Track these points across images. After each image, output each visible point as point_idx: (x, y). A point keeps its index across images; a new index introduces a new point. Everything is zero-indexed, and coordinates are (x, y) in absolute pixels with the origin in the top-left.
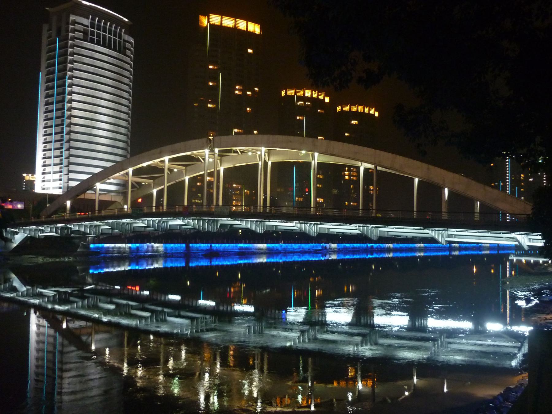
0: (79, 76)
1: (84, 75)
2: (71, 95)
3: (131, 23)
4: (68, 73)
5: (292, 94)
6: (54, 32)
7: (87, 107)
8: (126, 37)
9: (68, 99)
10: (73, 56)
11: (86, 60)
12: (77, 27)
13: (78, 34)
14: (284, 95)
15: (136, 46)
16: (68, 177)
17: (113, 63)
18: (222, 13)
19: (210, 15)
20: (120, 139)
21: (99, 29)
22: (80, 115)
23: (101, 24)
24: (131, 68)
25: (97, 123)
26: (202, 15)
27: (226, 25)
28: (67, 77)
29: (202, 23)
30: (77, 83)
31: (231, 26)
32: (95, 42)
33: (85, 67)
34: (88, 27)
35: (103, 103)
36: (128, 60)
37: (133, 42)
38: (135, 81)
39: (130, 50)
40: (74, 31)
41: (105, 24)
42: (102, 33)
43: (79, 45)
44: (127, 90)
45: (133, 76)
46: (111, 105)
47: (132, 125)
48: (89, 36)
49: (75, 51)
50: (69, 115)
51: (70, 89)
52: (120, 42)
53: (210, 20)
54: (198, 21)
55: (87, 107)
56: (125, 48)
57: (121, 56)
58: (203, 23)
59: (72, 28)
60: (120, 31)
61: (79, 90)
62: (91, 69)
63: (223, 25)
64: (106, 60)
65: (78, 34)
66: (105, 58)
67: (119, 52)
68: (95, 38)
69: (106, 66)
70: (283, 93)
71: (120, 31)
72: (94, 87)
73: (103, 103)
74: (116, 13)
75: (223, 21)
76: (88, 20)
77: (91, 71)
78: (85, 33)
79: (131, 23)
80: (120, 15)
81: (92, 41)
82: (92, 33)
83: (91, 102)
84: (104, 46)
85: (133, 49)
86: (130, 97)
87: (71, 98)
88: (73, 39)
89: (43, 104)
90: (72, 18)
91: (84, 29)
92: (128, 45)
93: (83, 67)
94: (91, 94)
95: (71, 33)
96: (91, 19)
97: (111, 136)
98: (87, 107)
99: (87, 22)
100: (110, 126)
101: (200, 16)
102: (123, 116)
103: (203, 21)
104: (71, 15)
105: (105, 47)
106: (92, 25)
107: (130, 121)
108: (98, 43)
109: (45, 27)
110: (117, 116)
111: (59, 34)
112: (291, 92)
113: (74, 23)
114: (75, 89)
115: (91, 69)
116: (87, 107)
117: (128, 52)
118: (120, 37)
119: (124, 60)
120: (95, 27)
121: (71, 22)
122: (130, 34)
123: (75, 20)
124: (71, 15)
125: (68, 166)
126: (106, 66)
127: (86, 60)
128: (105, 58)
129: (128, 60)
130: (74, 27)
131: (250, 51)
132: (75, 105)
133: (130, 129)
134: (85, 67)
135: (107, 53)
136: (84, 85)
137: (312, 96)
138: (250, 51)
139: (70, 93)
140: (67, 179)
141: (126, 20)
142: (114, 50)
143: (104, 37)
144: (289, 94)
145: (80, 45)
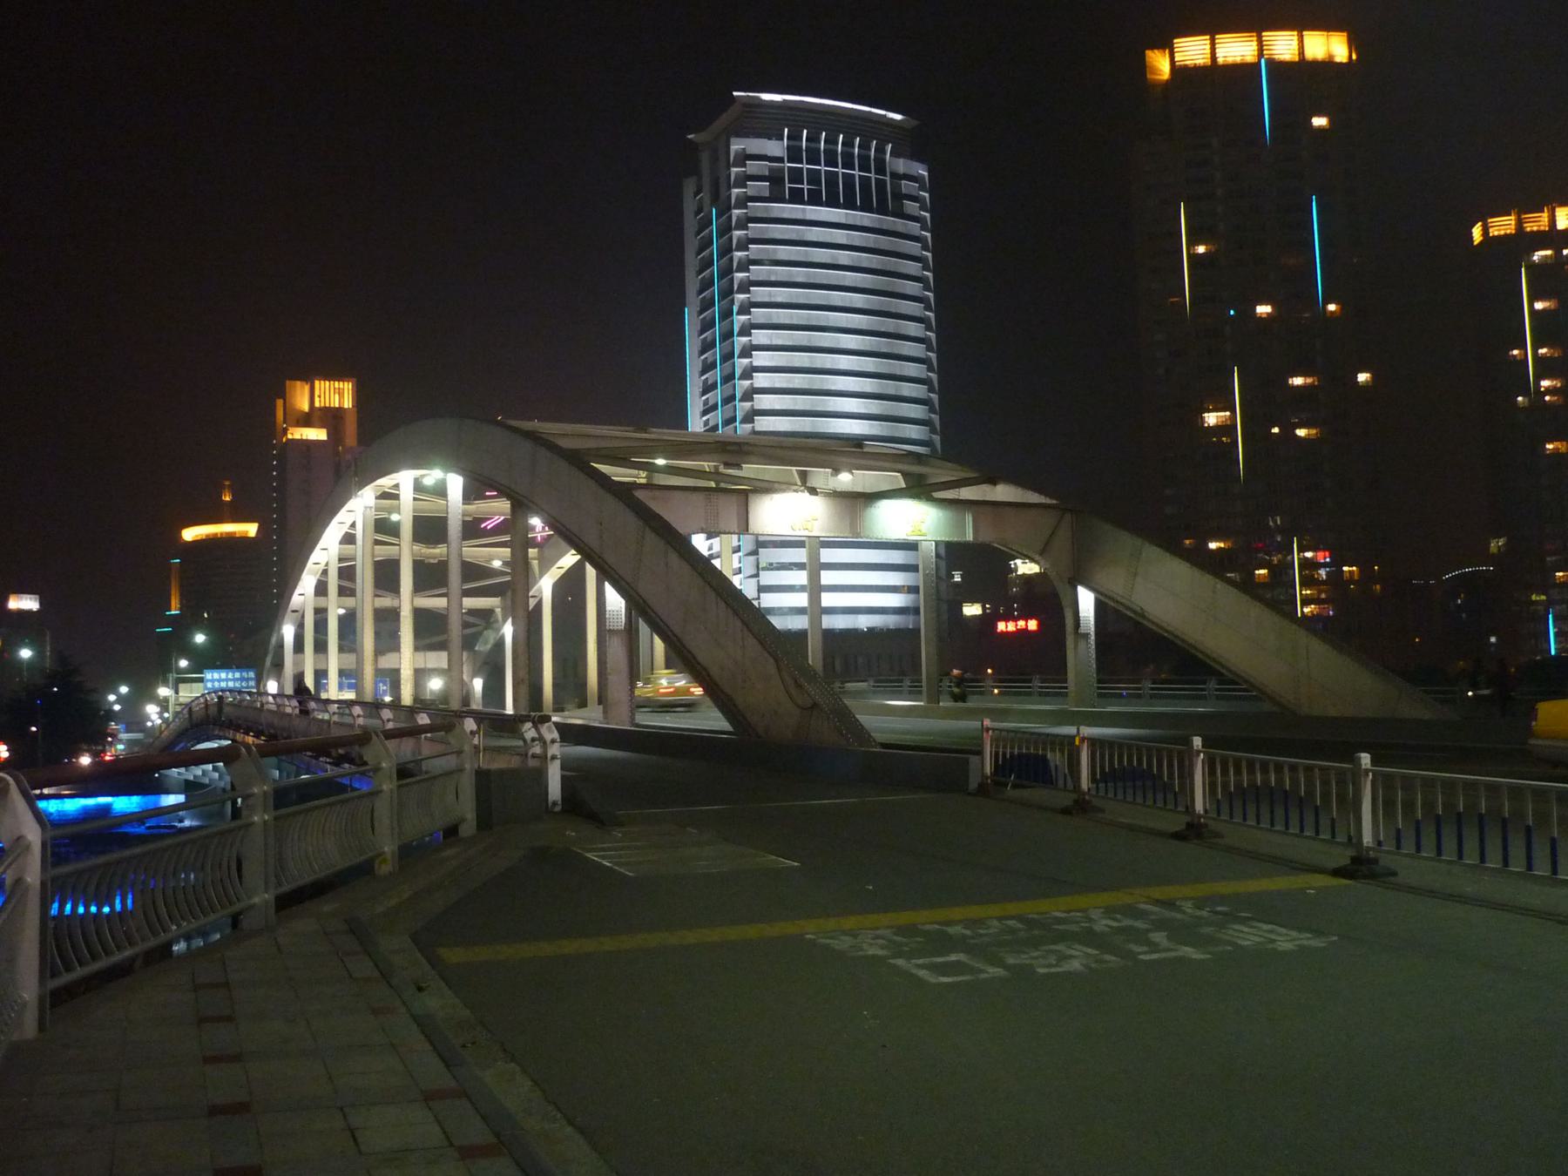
0: (766, 299)
1: (781, 294)
2: (750, 356)
3: (914, 123)
4: (738, 298)
5: (1542, 228)
6: (705, 195)
7: (798, 381)
8: (901, 165)
9: (743, 366)
10: (747, 249)
11: (784, 252)
12: (753, 167)
13: (754, 187)
14: (1481, 238)
15: (935, 186)
16: (758, 581)
17: (864, 245)
18: (1213, 27)
19: (1175, 41)
20: (913, 415)
21: (831, 162)
22: (777, 407)
23: (820, 143)
24: (925, 248)
25: (827, 422)
26: (1152, 48)
27: (1230, 60)
28: (735, 309)
29: (1155, 71)
30: (762, 321)
31: (35, 610)
32: (806, 198)
33: (781, 272)
34: (783, 162)
35: (844, 362)
36: (914, 228)
37: (926, 174)
38: (941, 266)
39: (914, 199)
40: (743, 180)
41: (831, 141)
42: (840, 170)
43: (759, 215)
44: (920, 275)
45: (932, 232)
46: (868, 364)
47: (941, 372)
48: (787, 185)
49: (751, 234)
50: (748, 412)
51: (744, 339)
52: (881, 185)
53: (1178, 57)
54: (1142, 66)
55: (797, 381)
56: (899, 197)
57: (890, 222)
58: (1161, 70)
59: (737, 173)
60: (880, 150)
61: (770, 337)
62: (799, 274)
63: (1220, 61)
64: (843, 241)
65: (754, 187)
66: (840, 236)
67: (882, 210)
68: (805, 187)
69: (844, 257)
70: (1477, 233)
71: (880, 150)
72: (814, 323)
73: (844, 362)
74: (863, 105)
75: (1217, 51)
76: (780, 142)
77: (800, 279)
78: (775, 179)
79: (914, 123)
80: (874, 107)
81: (796, 197)
82: (796, 176)
83: (807, 365)
84: (832, 202)
85: (928, 234)
86: (933, 416)
87: (751, 362)
88: (743, 202)
89: (699, 367)
90: (736, 146)
91: (771, 169)
92: (907, 186)
93: (776, 273)
94: (805, 343)
95: (736, 187)
96: (788, 138)
97: (884, 433)
98: (798, 381)
99: (776, 148)
100: (871, 425)
101: (1149, 53)
102: (912, 369)
103: (1155, 63)
104: (733, 140)
105: (854, 208)
106: (794, 154)
107: (939, 446)
108: (815, 200)
109: (689, 187)
110: (891, 392)
111: (715, 198)
112: (1503, 225)
113: (744, 157)
114: (760, 336)
115: (799, 274)
116: (797, 381)
117: (911, 207)
118: (881, 169)
119: (900, 229)
120: (820, 161)
121: (735, 158)
122: (916, 156)
123: (744, 149)
124: (733, 140)
125: (755, 553)
126: (844, 257)
127: (784, 252)
128: (840, 236)
129: (914, 228)
130: (743, 169)
131: (1319, 121)
132: (761, 380)
133: (936, 385)
134: (781, 272)
135: (843, 221)
136: (782, 321)
137: (1555, 225)
138: (1319, 121)
139: (747, 352)
140: (757, 588)
141: (898, 117)
142: (866, 207)
143: (832, 177)
144: (1494, 232)
145: (765, 215)
